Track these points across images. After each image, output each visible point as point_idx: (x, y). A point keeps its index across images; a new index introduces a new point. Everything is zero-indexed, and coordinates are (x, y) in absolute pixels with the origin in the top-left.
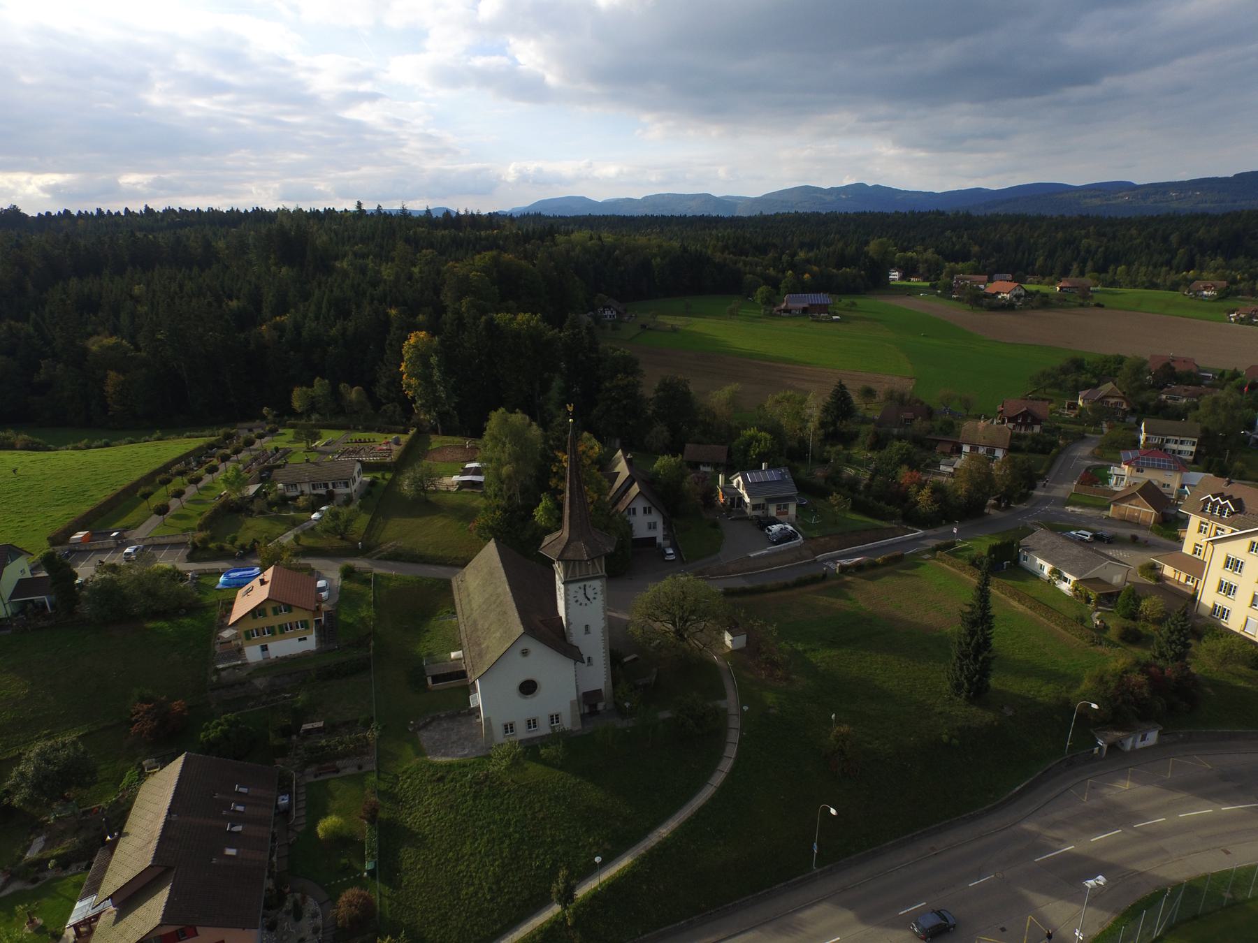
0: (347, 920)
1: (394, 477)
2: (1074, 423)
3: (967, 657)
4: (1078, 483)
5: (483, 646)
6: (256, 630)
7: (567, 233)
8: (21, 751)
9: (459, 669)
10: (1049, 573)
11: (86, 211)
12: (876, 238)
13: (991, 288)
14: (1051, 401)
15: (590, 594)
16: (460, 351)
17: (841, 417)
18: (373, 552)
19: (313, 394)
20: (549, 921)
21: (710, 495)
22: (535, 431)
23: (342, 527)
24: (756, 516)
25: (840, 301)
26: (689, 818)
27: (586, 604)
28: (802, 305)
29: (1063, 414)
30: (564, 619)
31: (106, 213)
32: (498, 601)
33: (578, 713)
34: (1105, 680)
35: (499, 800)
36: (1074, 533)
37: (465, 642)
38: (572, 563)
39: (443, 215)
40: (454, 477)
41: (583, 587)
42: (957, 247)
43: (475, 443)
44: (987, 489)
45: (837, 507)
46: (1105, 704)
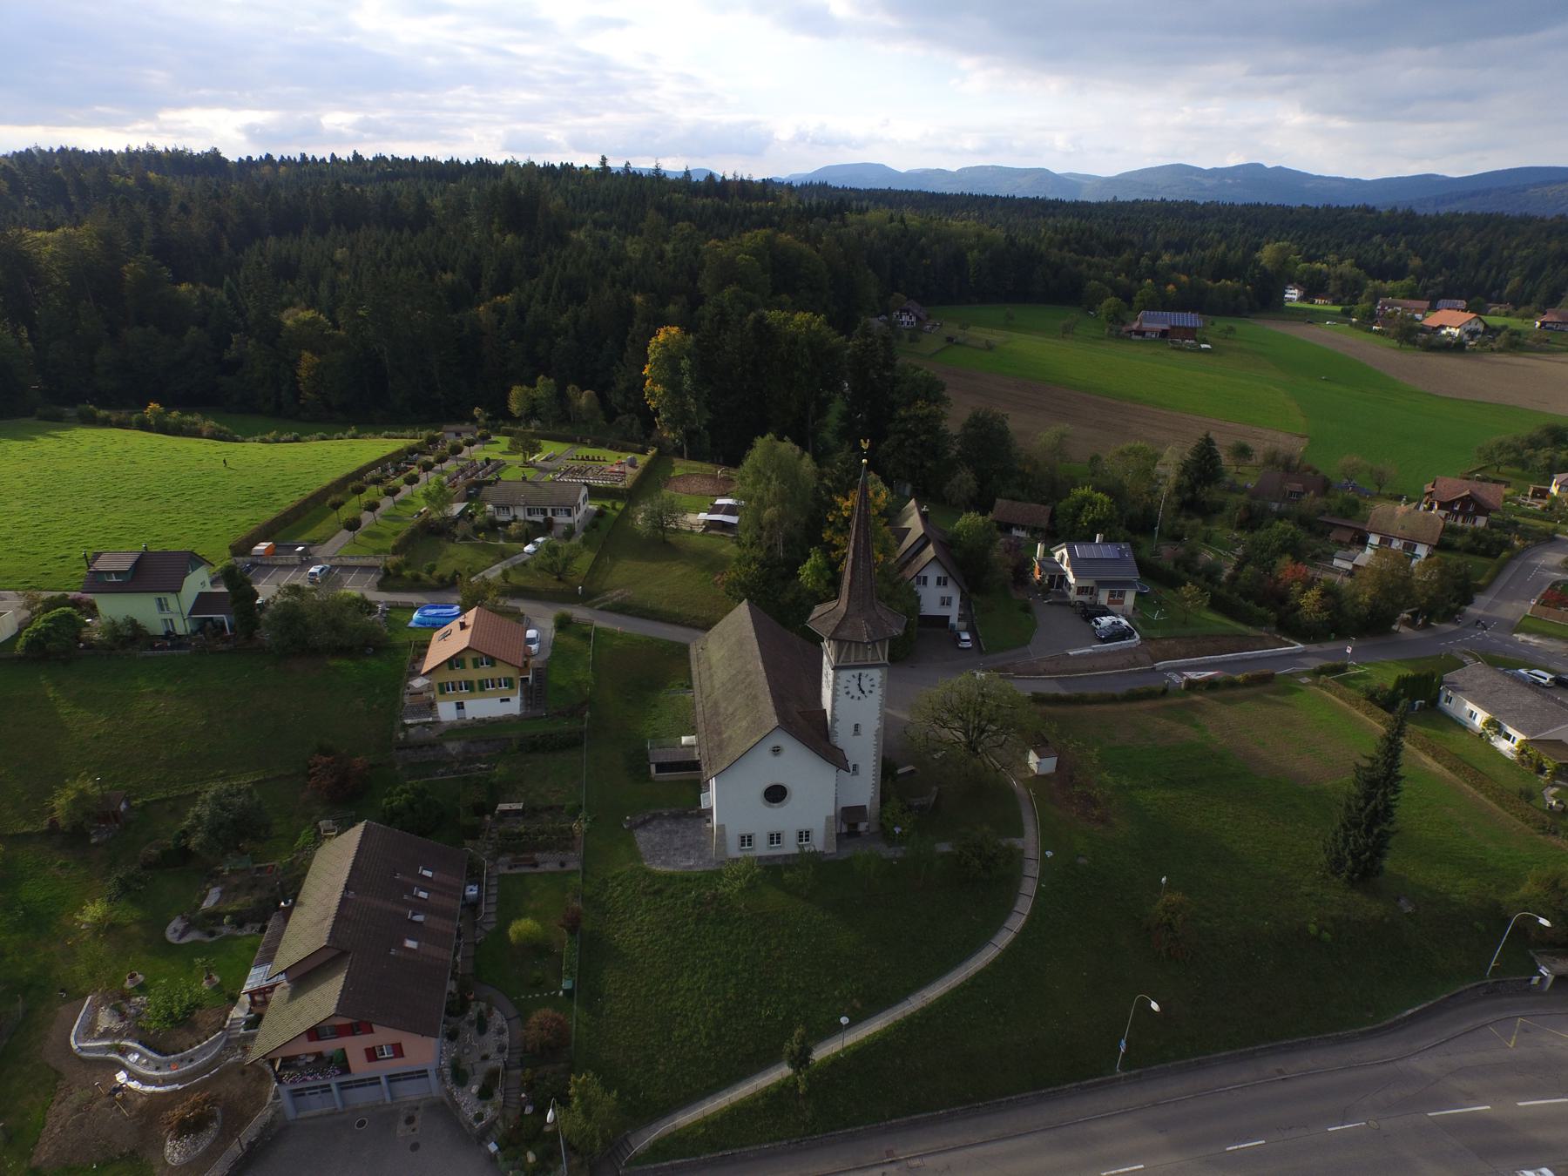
0: (538, 1045)
1: (626, 508)
2: (1541, 518)
3: (1357, 825)
4: (1538, 603)
5: (724, 736)
6: (453, 683)
7: (861, 211)
8: (197, 789)
9: (690, 759)
10: (1484, 724)
11: (289, 157)
12: (1272, 240)
13: (1433, 320)
14: (1508, 485)
15: (866, 686)
16: (718, 355)
17: (1202, 482)
18: (595, 600)
19: (535, 396)
20: (777, 1085)
21: (1023, 569)
22: (807, 464)
23: (560, 566)
24: (1082, 602)
25: (1213, 324)
26: (962, 983)
27: (859, 698)
29: (1524, 504)
30: (828, 713)
31: (310, 159)
32: (748, 680)
33: (834, 832)
34: (1561, 886)
35: (728, 928)
36: (1522, 671)
37: (701, 728)
38: (847, 644)
39: (706, 179)
40: (701, 514)
41: (857, 676)
42: (1388, 258)
43: (728, 473)
44: (1402, 599)
45: (1190, 602)
46: (1559, 920)
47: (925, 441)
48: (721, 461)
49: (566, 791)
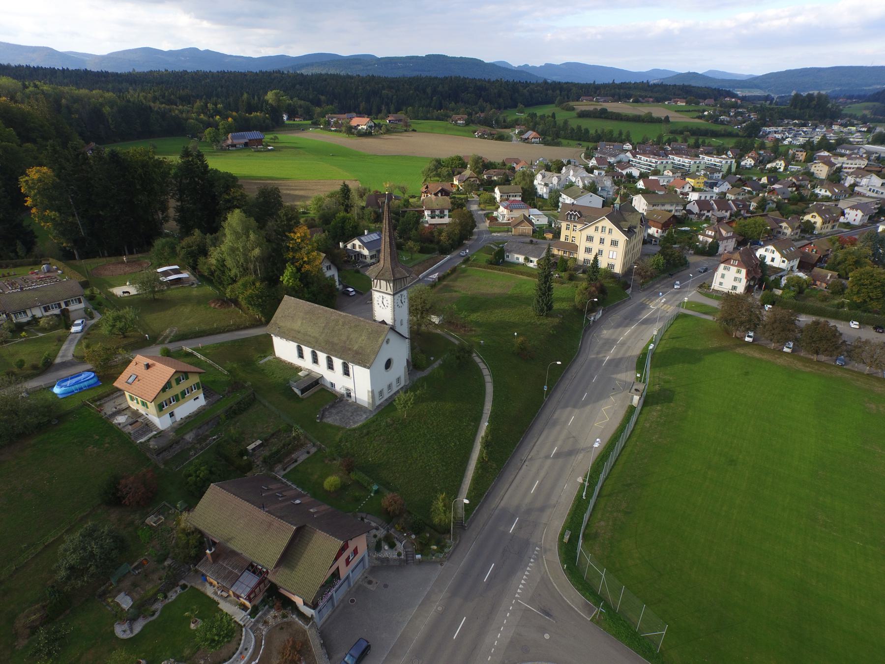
28: (243, 141)
48: (106, 254)
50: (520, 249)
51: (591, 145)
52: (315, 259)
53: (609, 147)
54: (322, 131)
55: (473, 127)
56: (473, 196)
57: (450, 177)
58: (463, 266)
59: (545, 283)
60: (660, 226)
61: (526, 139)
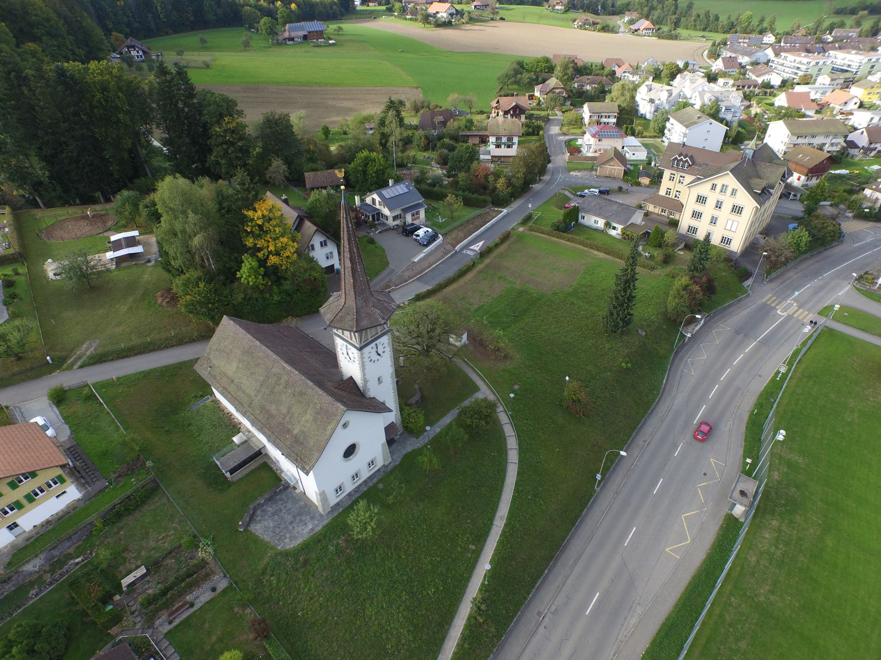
47: (242, 146)
49: (172, 532)
50: (600, 208)
51: (719, 37)
52: (284, 248)
53: (744, 43)
54: (397, 19)
55: (572, 15)
56: (557, 112)
57: (531, 85)
58: (521, 229)
59: (625, 290)
60: (806, 171)
61: (636, 31)
